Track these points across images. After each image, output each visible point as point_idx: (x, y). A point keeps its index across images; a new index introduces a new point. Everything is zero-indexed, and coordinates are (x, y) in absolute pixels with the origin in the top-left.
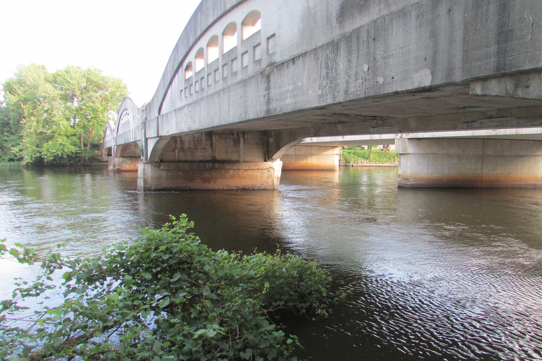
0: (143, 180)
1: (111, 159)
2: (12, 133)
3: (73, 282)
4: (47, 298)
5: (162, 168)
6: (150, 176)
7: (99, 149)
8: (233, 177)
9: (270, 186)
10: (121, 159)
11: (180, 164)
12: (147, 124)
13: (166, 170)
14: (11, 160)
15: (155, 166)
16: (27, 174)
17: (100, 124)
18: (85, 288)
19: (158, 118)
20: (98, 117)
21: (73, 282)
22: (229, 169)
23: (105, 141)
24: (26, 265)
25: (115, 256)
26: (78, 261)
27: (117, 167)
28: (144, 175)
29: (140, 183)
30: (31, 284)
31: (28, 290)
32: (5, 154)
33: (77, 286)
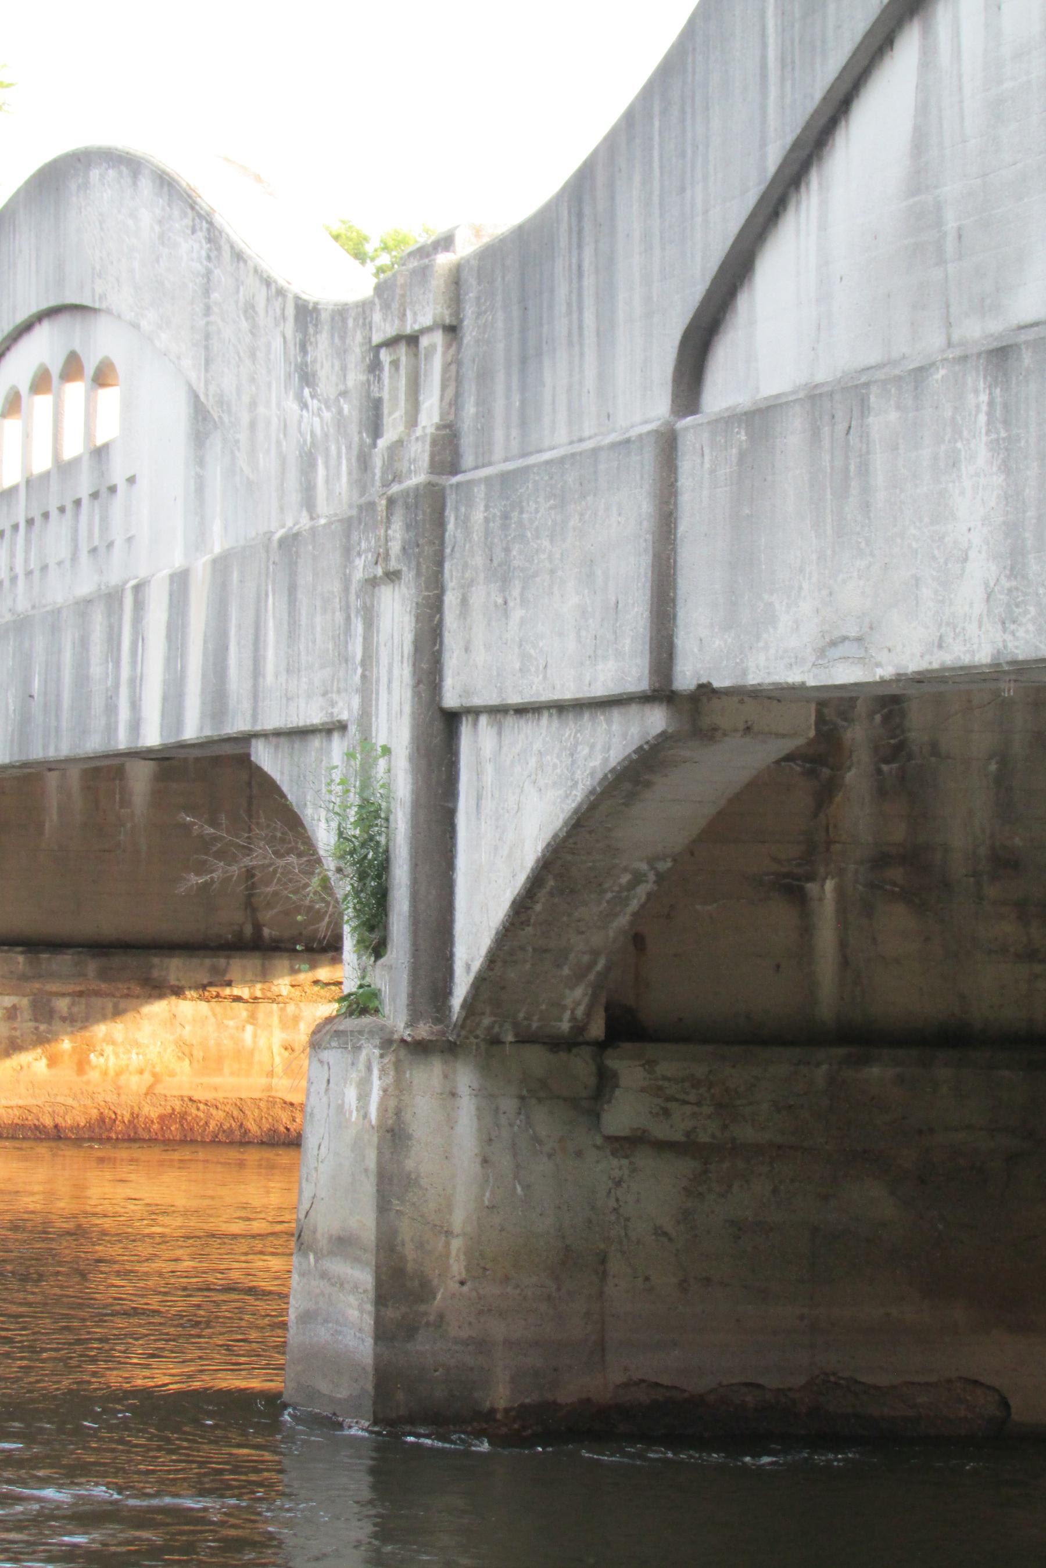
0: (365, 1277)
6: (459, 1219)
28: (383, 1206)
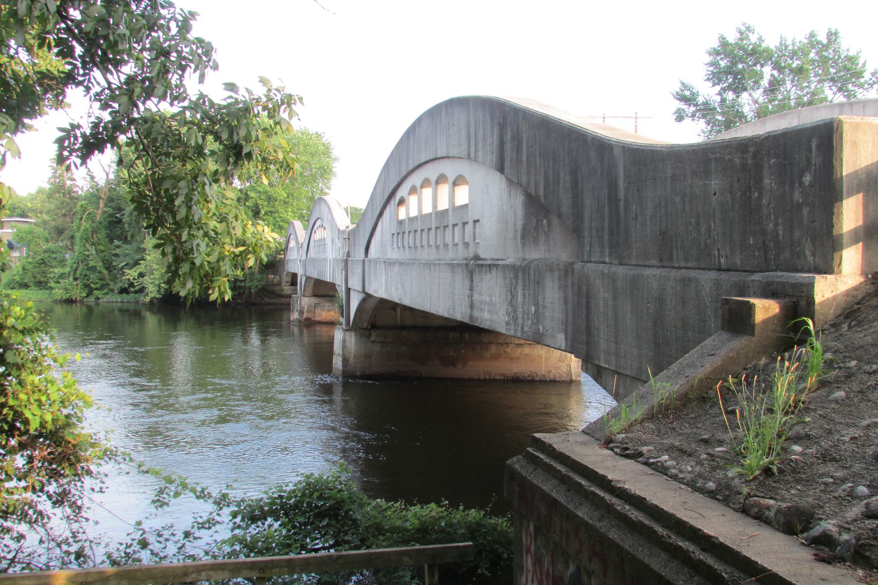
1: (295, 300)
2: (125, 240)
3: (238, 520)
4: (216, 532)
5: (373, 338)
6: (353, 351)
7: (277, 271)
8: (495, 357)
9: (564, 375)
10: (314, 300)
11: (404, 333)
12: (350, 264)
13: (380, 342)
14: (124, 291)
15: (362, 335)
16: (151, 320)
17: (279, 226)
18: (248, 526)
19: (364, 261)
20: (277, 212)
21: (238, 520)
22: (490, 343)
23: (287, 258)
24: (202, 501)
25: (276, 498)
26: (243, 501)
27: (305, 315)
28: (343, 350)
29: (337, 363)
30: (205, 518)
31: (203, 523)
32: (114, 279)
33: (241, 524)
